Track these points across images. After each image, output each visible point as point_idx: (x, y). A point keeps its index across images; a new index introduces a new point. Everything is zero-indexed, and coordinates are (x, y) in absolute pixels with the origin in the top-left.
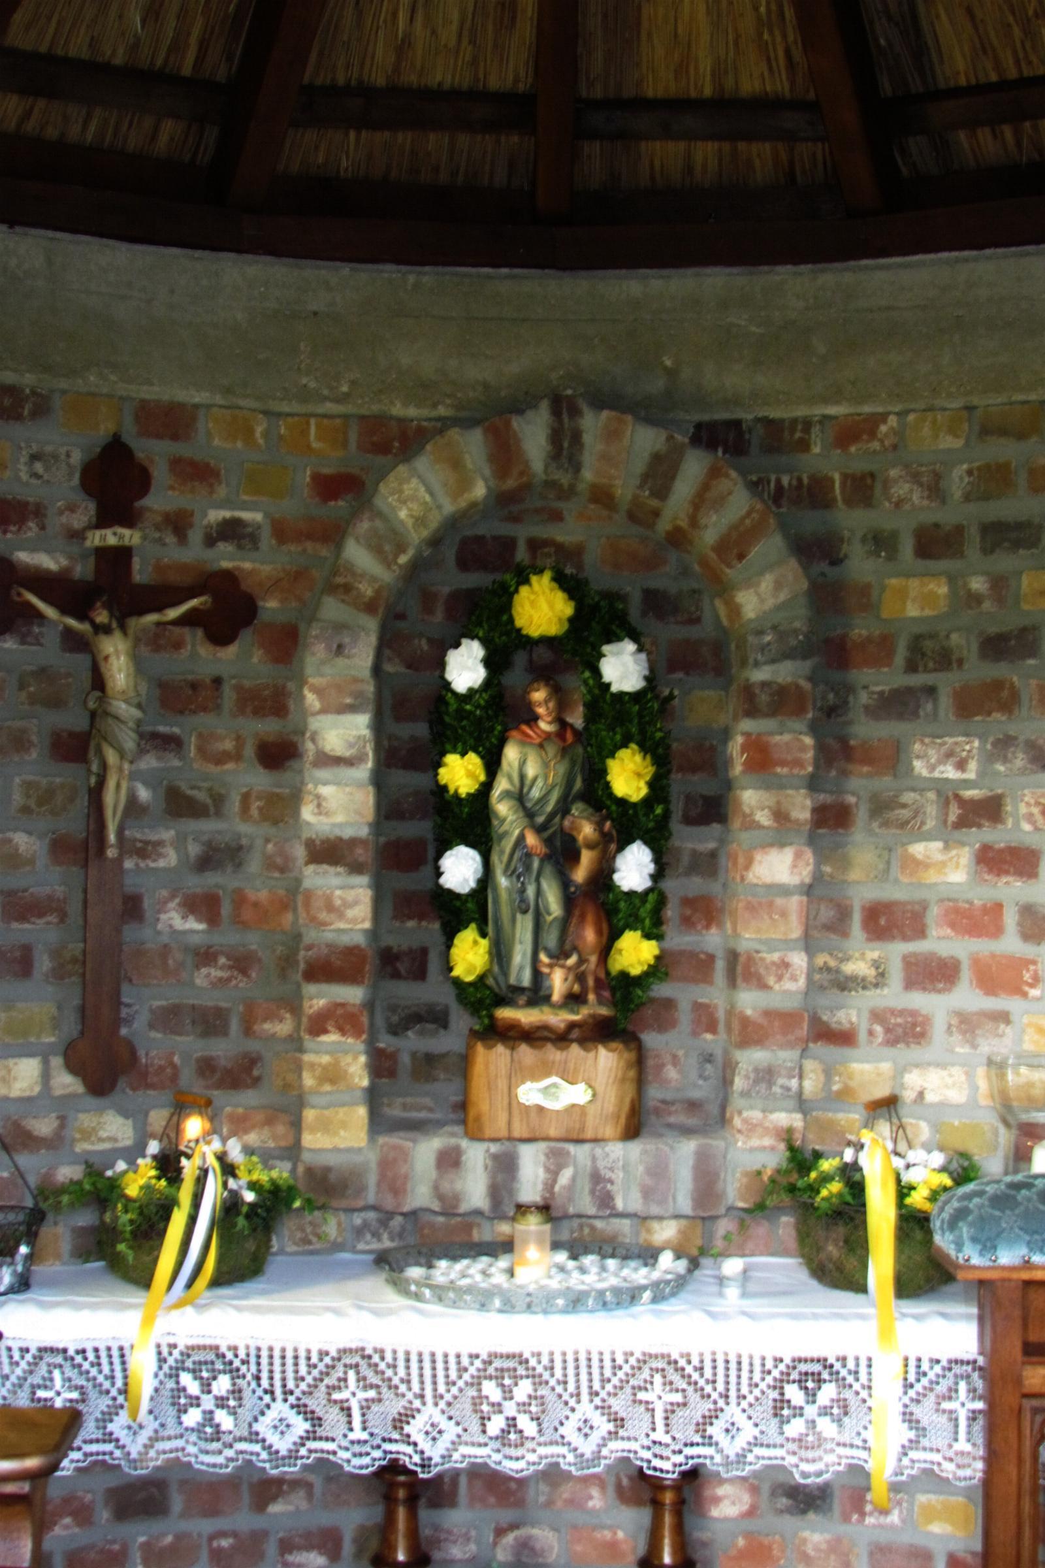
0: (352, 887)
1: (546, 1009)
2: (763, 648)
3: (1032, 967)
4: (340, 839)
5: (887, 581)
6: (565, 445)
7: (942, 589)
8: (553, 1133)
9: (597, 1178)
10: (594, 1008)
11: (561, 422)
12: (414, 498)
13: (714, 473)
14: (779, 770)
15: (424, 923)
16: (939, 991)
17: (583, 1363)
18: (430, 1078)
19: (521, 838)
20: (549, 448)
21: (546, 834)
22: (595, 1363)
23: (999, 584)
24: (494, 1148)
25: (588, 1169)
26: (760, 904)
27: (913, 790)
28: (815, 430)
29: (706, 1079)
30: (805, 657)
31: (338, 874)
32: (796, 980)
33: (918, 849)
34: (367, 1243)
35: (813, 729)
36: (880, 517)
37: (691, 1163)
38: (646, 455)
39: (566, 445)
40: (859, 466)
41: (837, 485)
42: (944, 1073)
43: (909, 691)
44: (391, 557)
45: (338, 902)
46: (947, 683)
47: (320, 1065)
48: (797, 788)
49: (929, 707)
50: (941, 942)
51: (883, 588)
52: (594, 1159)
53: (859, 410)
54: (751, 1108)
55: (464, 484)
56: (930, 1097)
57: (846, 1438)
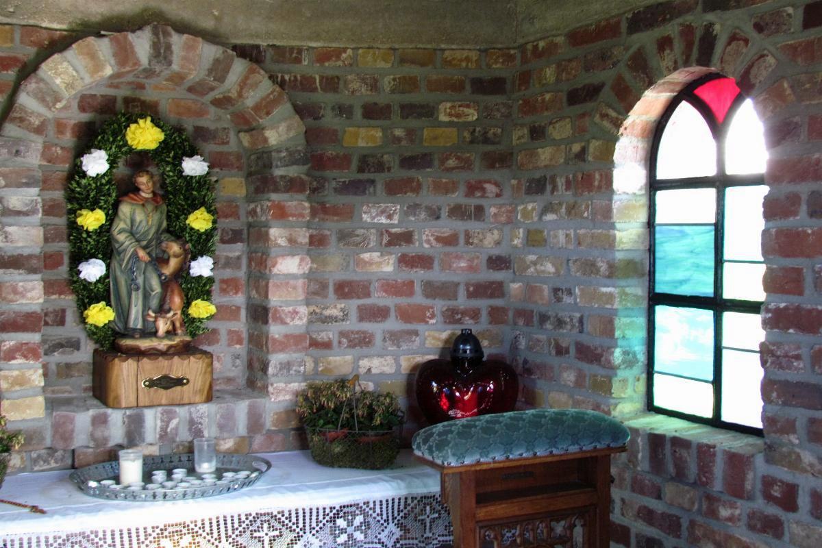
0: (31, 281)
1: (154, 339)
2: (280, 159)
3: (431, 310)
4: (22, 255)
5: (347, 129)
6: (161, 52)
7: (378, 134)
8: (164, 402)
9: (192, 422)
10: (181, 337)
11: (159, 39)
12: (65, 72)
13: (252, 71)
14: (291, 219)
15: (63, 297)
16: (379, 322)
17: (222, 522)
18: (68, 376)
19: (135, 254)
20: (152, 51)
21: (148, 250)
22: (229, 522)
23: (410, 133)
24: (128, 412)
25: (188, 418)
26: (281, 284)
27: (362, 228)
28: (304, 54)
29: (236, 367)
30: (304, 165)
31: (20, 274)
32: (302, 320)
33: (366, 256)
34: (41, 466)
35: (309, 199)
36: (343, 97)
37: (246, 411)
38: (211, 59)
39: (162, 51)
40: (330, 73)
41: (318, 81)
42: (382, 360)
43: (360, 181)
44: (51, 104)
45: (21, 289)
46: (381, 178)
47: (12, 376)
48: (302, 227)
49: (371, 189)
50: (378, 299)
51: (345, 132)
52: (190, 414)
53: (330, 45)
54: (280, 382)
55: (98, 67)
56: (374, 371)
57: (369, 539)
